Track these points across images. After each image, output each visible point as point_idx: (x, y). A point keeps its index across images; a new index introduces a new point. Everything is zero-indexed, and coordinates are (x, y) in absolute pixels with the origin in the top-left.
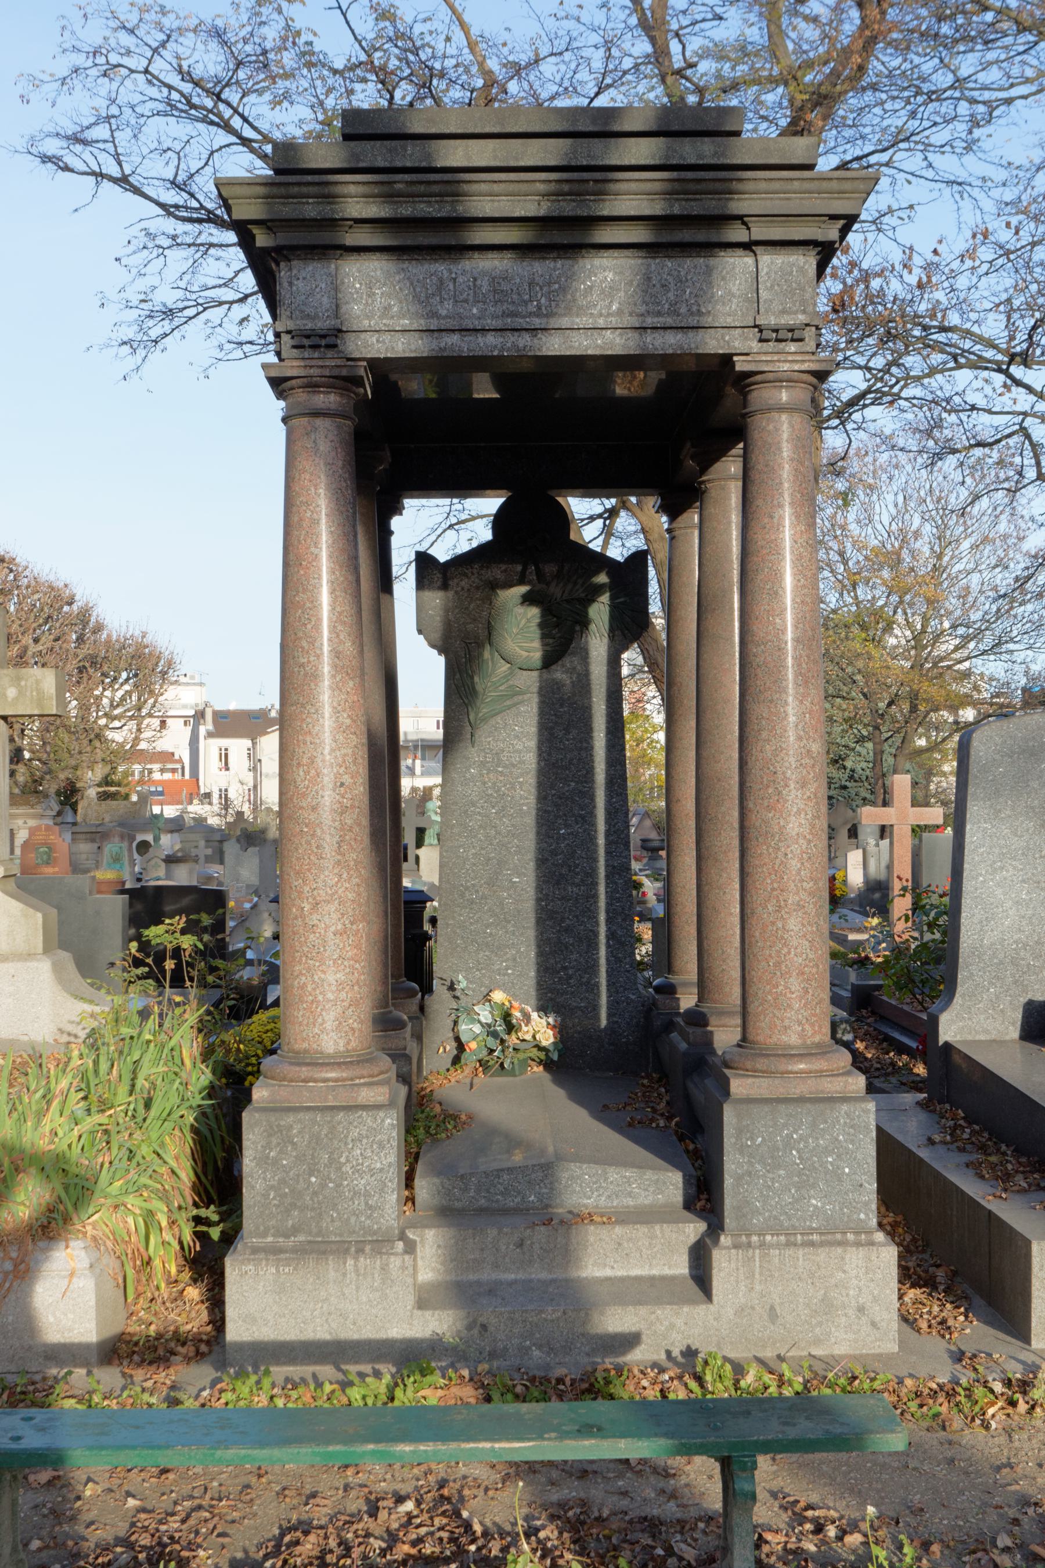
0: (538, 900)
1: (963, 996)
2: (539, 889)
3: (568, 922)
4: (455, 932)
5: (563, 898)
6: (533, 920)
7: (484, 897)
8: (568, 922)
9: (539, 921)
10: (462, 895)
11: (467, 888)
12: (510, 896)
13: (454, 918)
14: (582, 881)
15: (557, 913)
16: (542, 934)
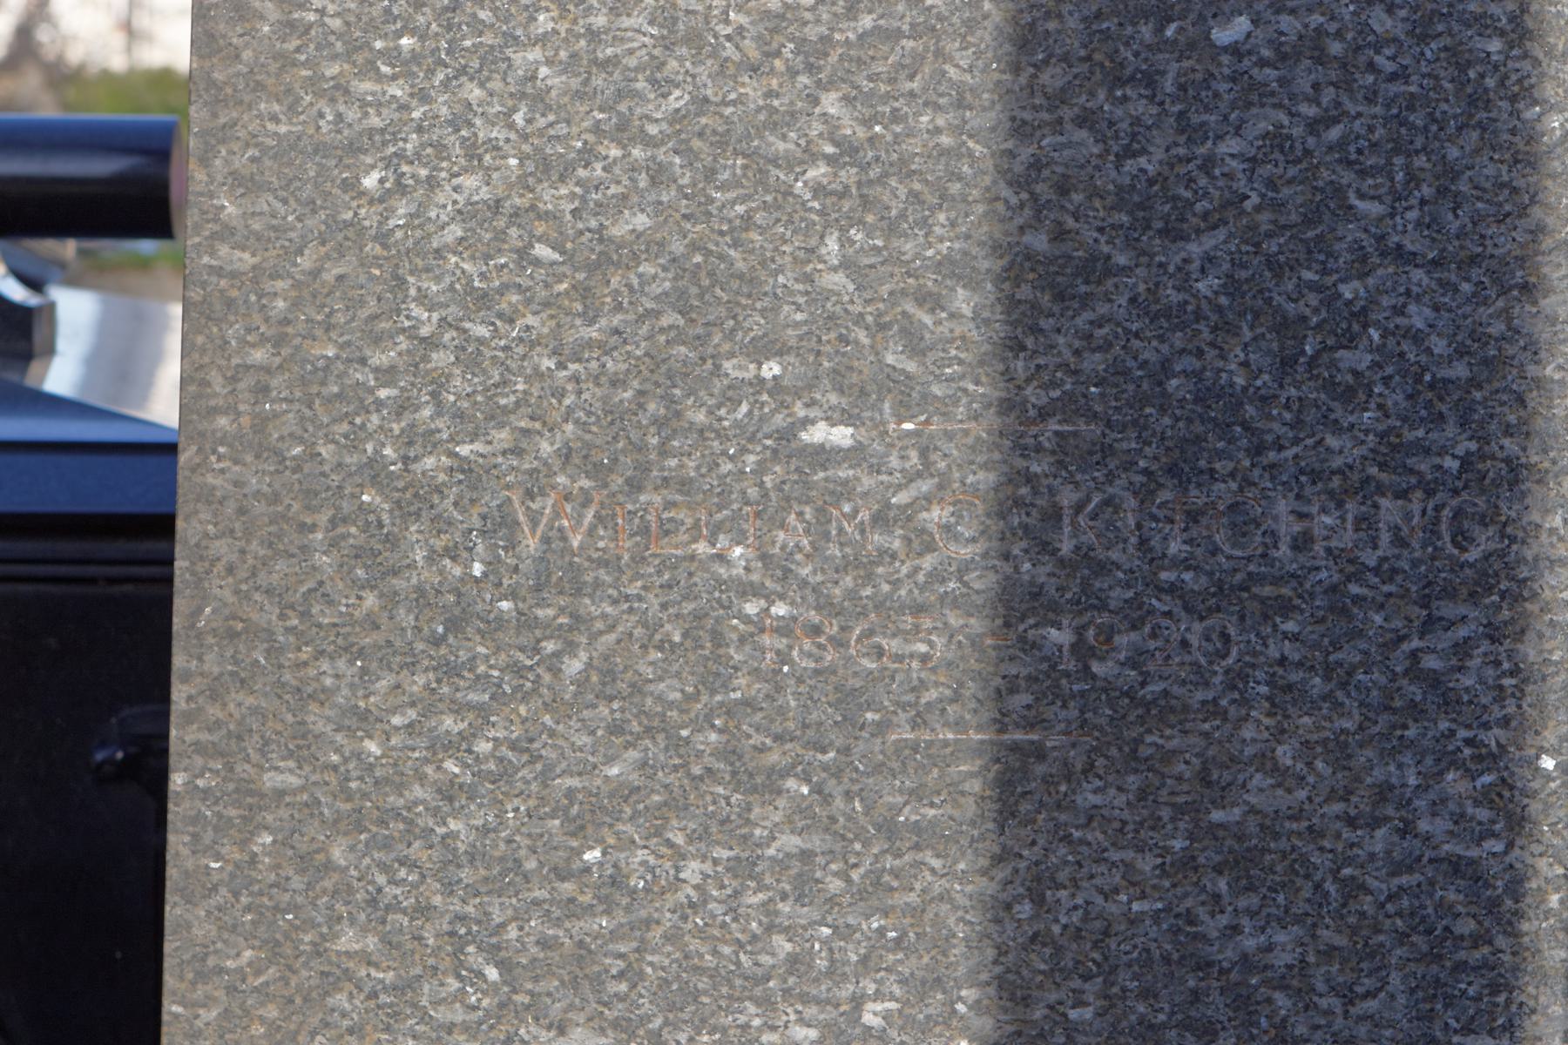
0: (1019, 607)
1: (186, 519)
2: (1023, 514)
3: (1259, 791)
4: (313, 864)
5: (1223, 592)
6: (970, 777)
7: (559, 575)
8: (1259, 791)
9: (1018, 784)
10: (376, 557)
11: (415, 500)
12: (778, 567)
13: (303, 747)
14: (1391, 452)
15: (1164, 711)
16: (1039, 886)
